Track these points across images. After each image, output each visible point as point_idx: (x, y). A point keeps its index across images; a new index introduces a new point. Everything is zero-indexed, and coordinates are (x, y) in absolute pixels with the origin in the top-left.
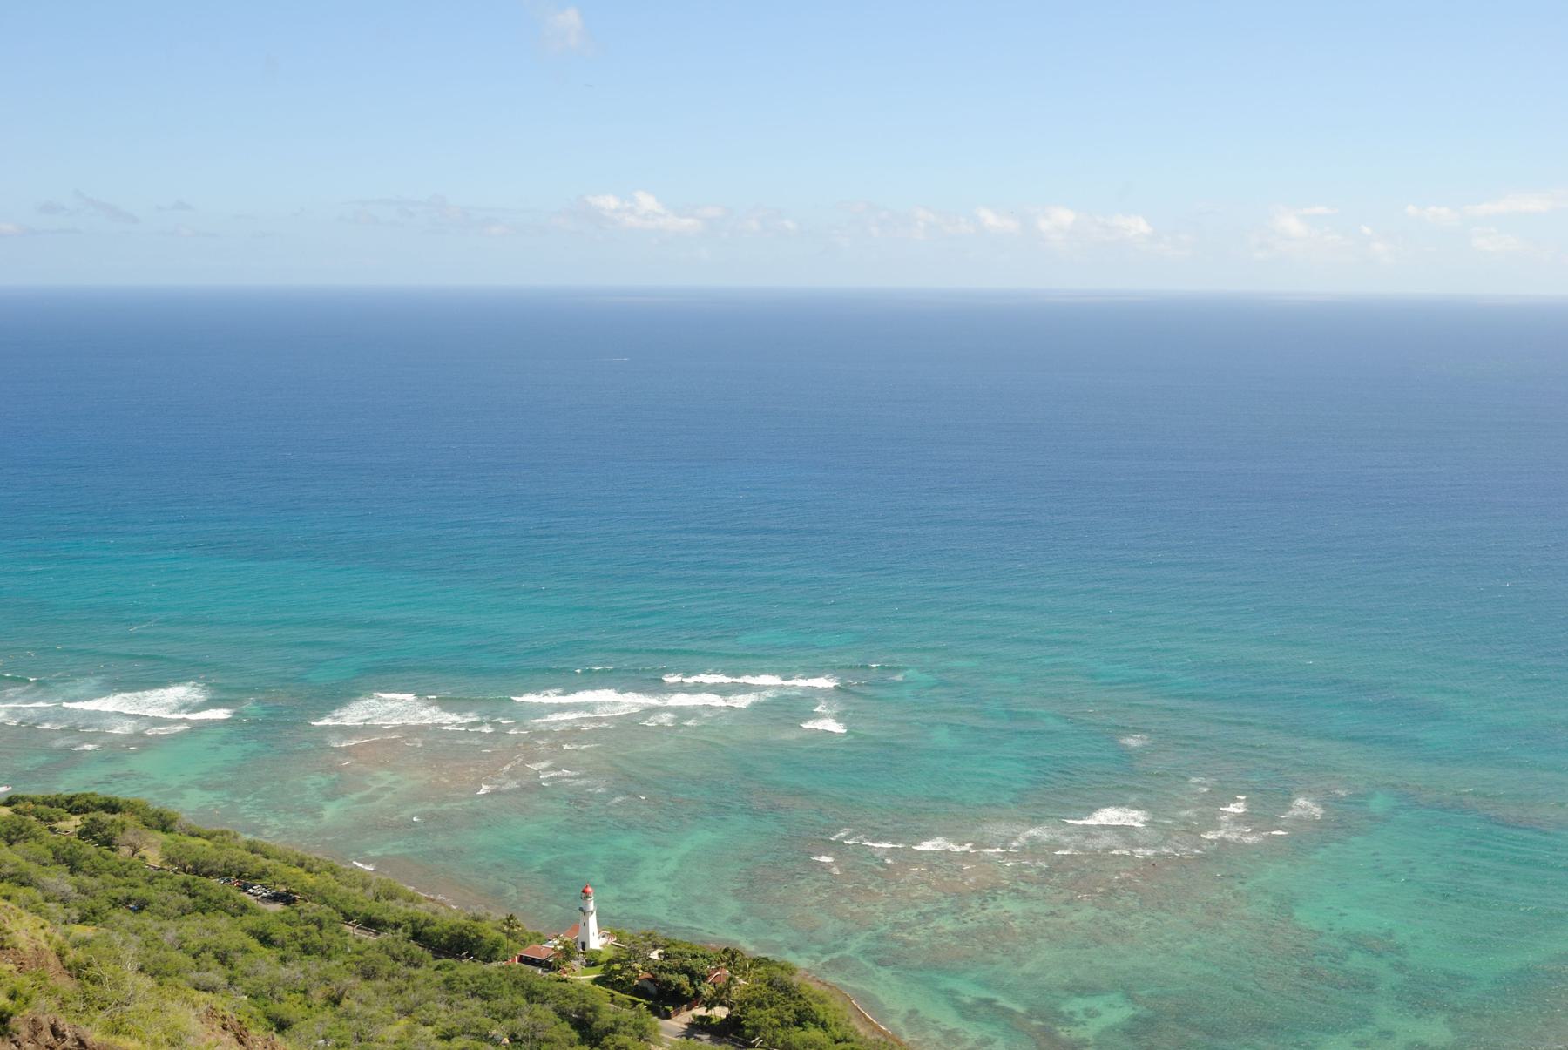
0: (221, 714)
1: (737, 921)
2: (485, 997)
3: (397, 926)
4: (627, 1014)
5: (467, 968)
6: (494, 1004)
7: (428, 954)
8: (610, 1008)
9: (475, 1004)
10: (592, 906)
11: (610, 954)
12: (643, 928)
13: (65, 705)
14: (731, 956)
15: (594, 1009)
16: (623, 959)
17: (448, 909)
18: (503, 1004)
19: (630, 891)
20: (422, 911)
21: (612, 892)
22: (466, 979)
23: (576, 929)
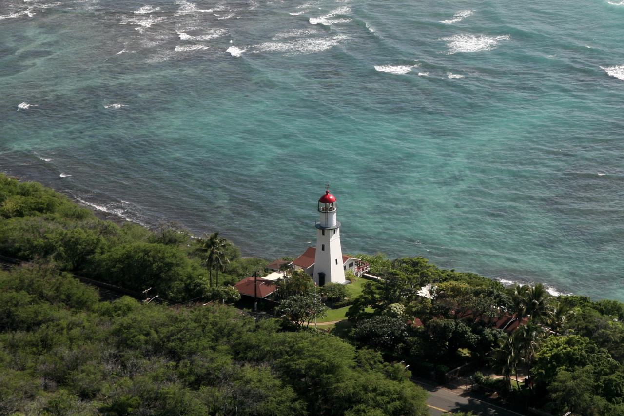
0: (445, 39)
1: (547, 243)
2: (174, 355)
3: (47, 250)
4: (376, 378)
5: (147, 313)
6: (184, 365)
7: (92, 293)
8: (355, 372)
9: (161, 364)
10: (334, 221)
11: (356, 290)
12: (409, 254)
13: (602, 68)
14: (531, 303)
15: (332, 369)
16: (387, 288)
17: (125, 222)
18: (201, 363)
19: (395, 201)
20: (80, 231)
21: (365, 203)
22: (146, 327)
23: (310, 253)
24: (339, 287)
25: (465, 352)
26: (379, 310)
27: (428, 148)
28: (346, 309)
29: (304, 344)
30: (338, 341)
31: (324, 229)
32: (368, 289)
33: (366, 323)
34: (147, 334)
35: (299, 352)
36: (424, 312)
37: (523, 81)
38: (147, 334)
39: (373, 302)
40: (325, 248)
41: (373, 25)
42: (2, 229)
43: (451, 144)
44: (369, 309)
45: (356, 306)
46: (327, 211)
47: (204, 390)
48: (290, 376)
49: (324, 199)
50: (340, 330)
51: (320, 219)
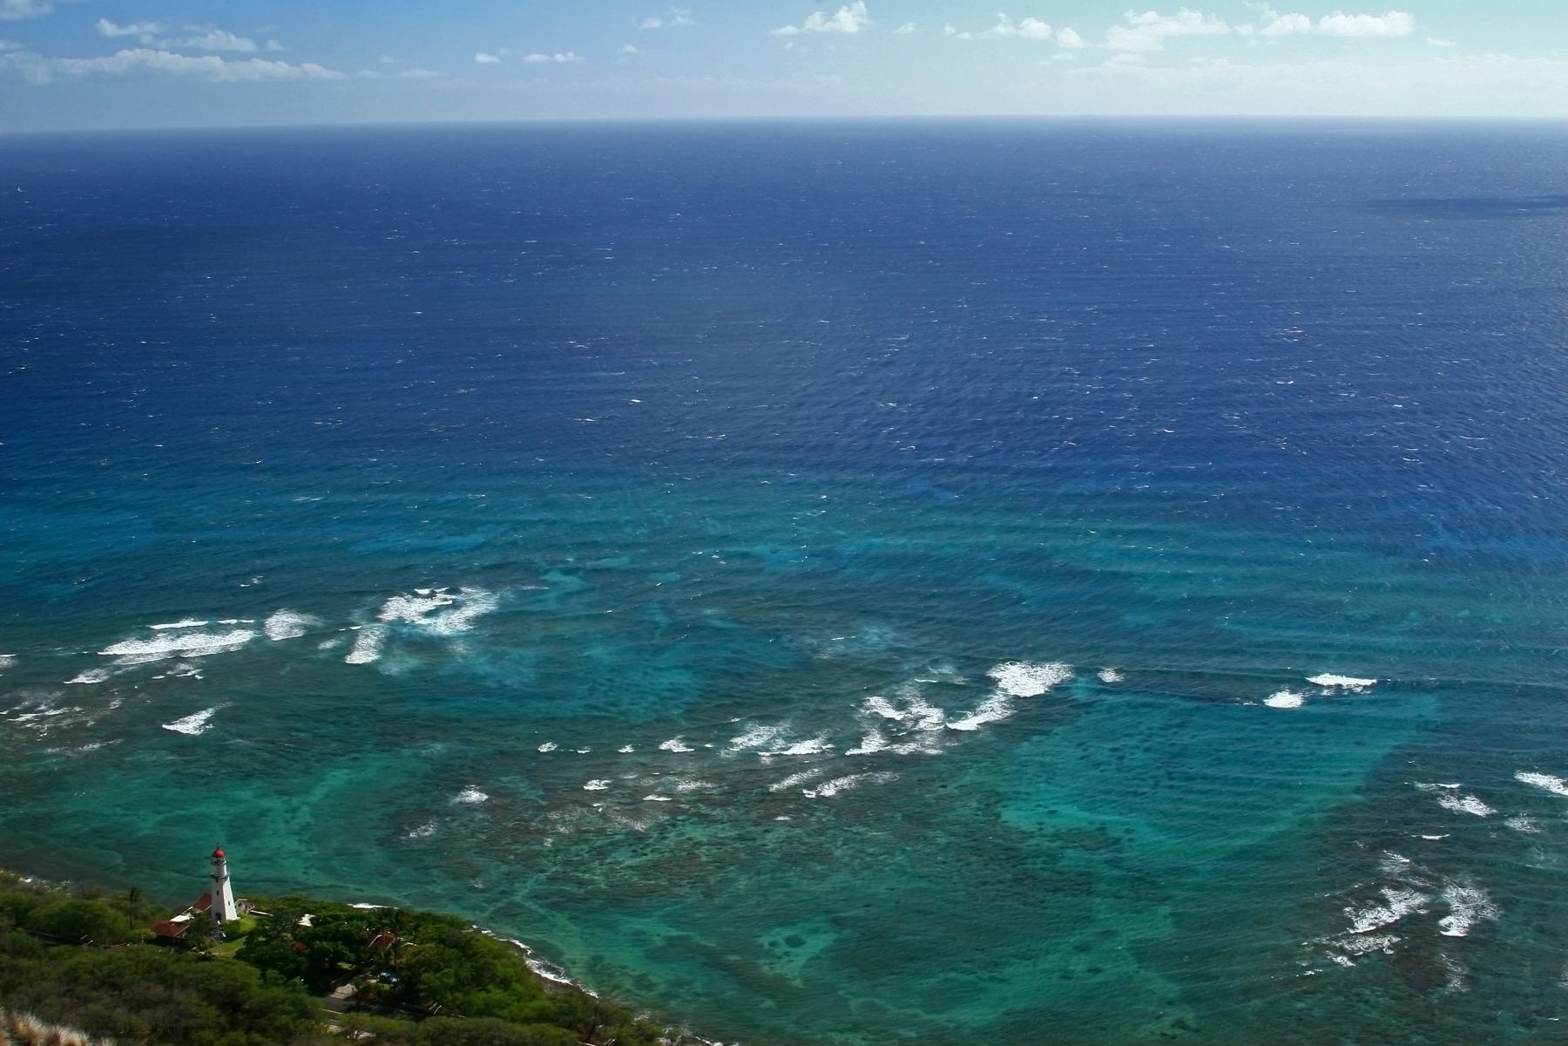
2: (114, 986)
15: (245, 987)
24: (236, 922)
25: (346, 966)
26: (270, 938)
27: (277, 803)
28: (244, 939)
29: (220, 971)
30: (242, 964)
31: (219, 879)
32: (261, 921)
33: (261, 948)
34: (92, 973)
35: (217, 977)
36: (308, 937)
37: (1444, 860)
38: (92, 973)
39: (264, 933)
40: (220, 893)
41: (1494, 901)
42: (9, 893)
43: (295, 802)
44: (262, 939)
45: (252, 934)
46: (218, 864)
47: (147, 1013)
48: (210, 996)
49: (216, 855)
50: (240, 956)
51: (212, 870)
